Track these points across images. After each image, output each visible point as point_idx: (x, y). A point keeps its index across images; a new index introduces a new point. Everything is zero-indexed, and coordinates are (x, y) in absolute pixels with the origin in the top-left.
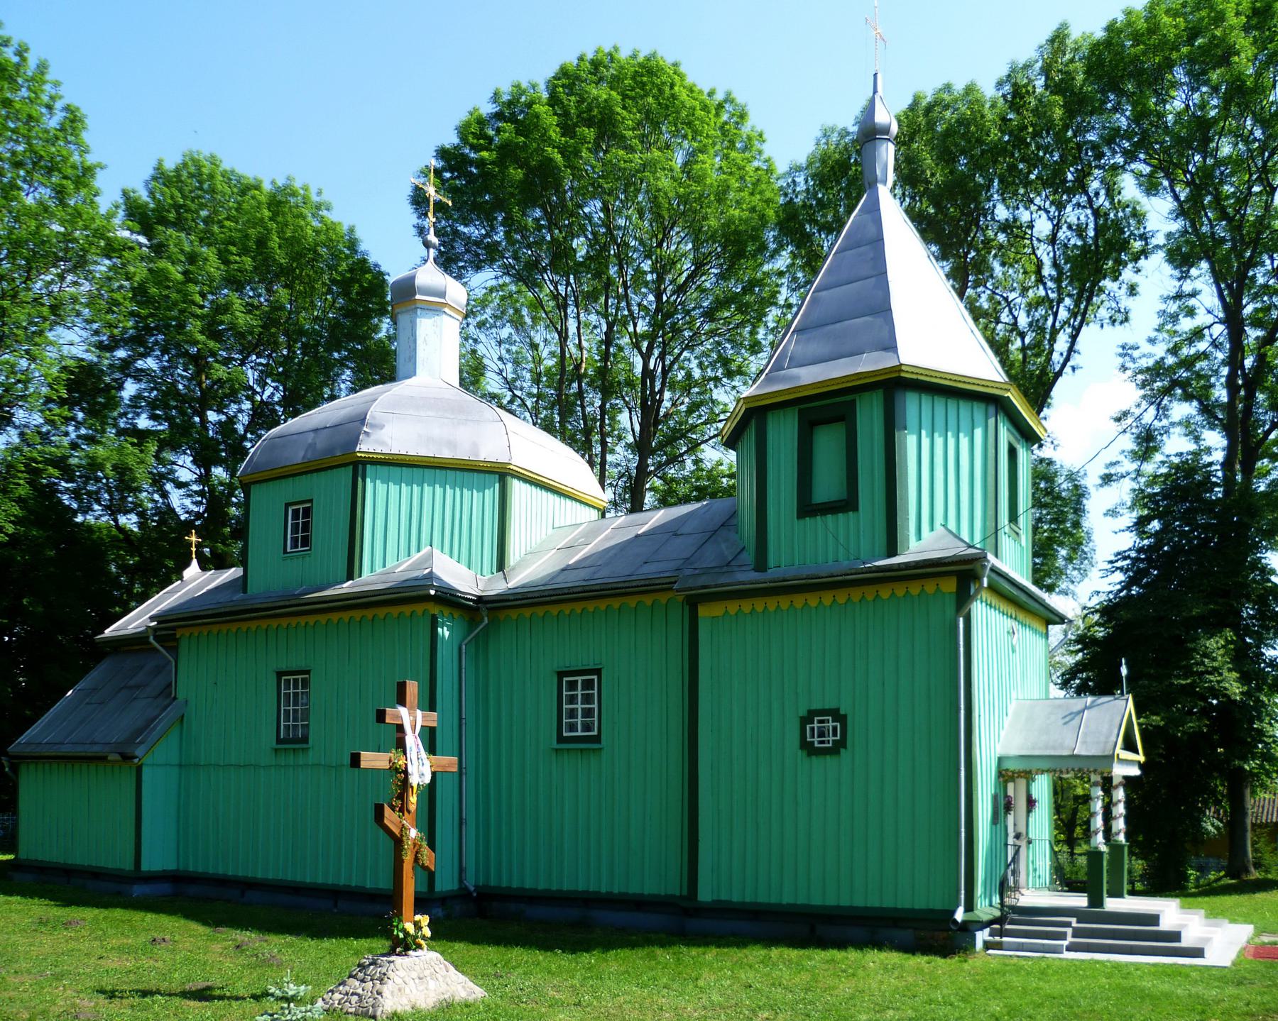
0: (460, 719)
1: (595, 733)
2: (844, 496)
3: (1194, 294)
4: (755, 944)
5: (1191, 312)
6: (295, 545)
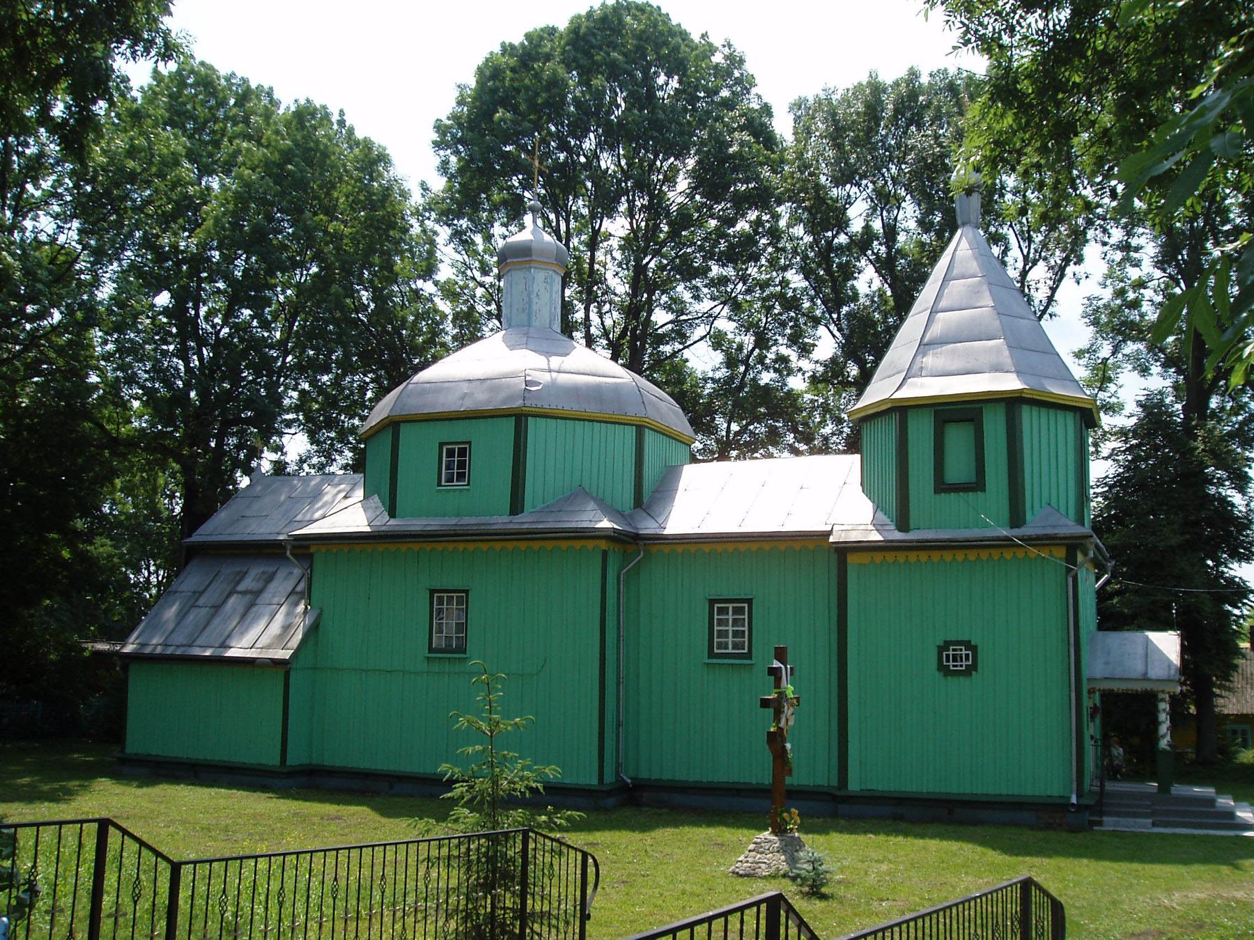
0: (619, 636)
1: (746, 651)
2: (974, 479)
3: (1137, 249)
4: (658, 827)
5: (1137, 264)
6: (450, 480)
